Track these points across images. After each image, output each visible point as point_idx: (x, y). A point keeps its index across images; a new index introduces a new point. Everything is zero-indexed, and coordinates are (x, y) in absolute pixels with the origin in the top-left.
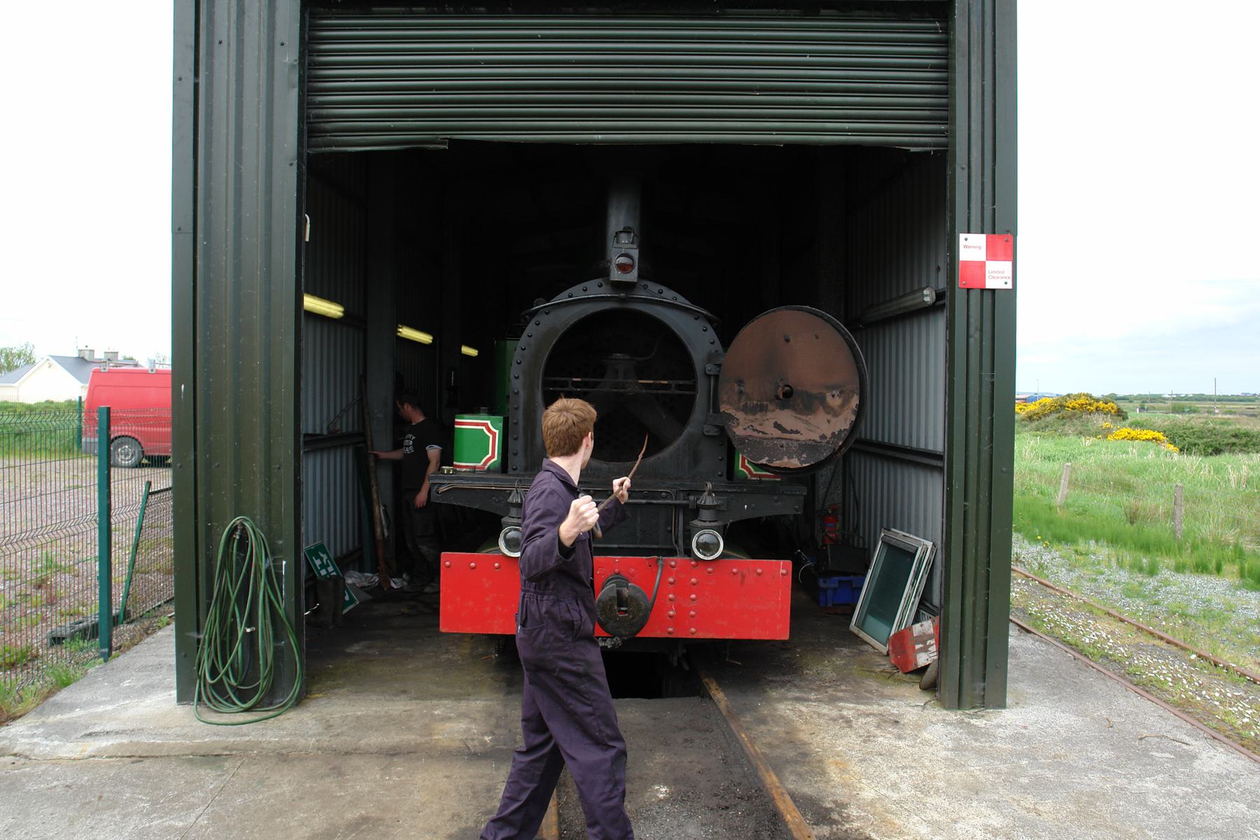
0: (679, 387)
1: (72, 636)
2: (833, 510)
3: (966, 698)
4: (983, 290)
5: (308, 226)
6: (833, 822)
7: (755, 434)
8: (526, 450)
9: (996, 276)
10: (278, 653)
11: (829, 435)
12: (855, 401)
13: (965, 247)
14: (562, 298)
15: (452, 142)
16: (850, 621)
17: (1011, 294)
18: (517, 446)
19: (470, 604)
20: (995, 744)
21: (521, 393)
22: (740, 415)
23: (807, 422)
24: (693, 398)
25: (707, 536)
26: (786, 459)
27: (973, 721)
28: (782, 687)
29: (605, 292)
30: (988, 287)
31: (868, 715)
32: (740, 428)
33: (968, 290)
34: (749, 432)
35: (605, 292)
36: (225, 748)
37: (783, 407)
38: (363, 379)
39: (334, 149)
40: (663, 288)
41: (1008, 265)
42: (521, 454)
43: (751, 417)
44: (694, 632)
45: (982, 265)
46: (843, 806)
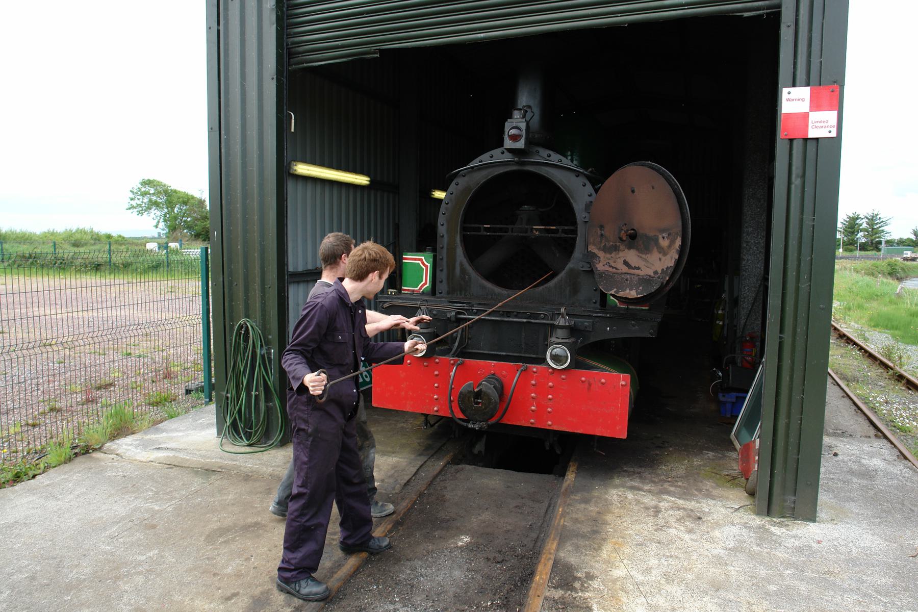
0: (565, 232)
1: (197, 390)
2: (752, 338)
3: (775, 507)
4: (806, 140)
5: (293, 121)
6: (573, 589)
7: (611, 269)
8: (448, 279)
9: (820, 125)
10: (268, 409)
11: (660, 272)
12: (678, 242)
13: (788, 100)
14: (475, 163)
15: (382, 51)
16: (731, 432)
17: (834, 144)
18: (442, 276)
19: (392, 388)
20: (774, 551)
21: (446, 236)
22: (601, 254)
23: (645, 260)
24: (574, 239)
25: (558, 349)
26: (628, 291)
27: (773, 529)
28: (628, 476)
29: (508, 157)
30: (810, 136)
31: (679, 509)
32: (601, 264)
33: (791, 140)
34: (607, 268)
35: (508, 157)
36: (220, 467)
37: (630, 248)
38: (397, 227)
39: (305, 65)
40: (551, 153)
41: (832, 116)
42: (445, 281)
43: (608, 256)
44: (549, 424)
45: (805, 116)
46: (590, 577)
